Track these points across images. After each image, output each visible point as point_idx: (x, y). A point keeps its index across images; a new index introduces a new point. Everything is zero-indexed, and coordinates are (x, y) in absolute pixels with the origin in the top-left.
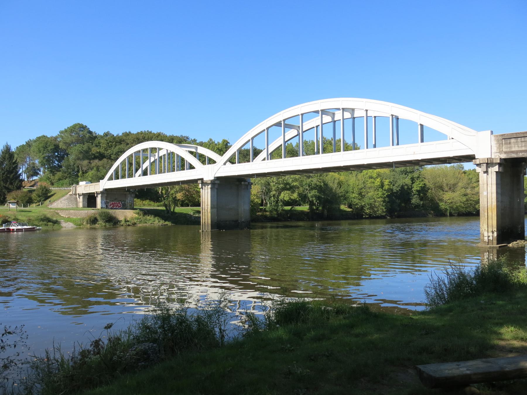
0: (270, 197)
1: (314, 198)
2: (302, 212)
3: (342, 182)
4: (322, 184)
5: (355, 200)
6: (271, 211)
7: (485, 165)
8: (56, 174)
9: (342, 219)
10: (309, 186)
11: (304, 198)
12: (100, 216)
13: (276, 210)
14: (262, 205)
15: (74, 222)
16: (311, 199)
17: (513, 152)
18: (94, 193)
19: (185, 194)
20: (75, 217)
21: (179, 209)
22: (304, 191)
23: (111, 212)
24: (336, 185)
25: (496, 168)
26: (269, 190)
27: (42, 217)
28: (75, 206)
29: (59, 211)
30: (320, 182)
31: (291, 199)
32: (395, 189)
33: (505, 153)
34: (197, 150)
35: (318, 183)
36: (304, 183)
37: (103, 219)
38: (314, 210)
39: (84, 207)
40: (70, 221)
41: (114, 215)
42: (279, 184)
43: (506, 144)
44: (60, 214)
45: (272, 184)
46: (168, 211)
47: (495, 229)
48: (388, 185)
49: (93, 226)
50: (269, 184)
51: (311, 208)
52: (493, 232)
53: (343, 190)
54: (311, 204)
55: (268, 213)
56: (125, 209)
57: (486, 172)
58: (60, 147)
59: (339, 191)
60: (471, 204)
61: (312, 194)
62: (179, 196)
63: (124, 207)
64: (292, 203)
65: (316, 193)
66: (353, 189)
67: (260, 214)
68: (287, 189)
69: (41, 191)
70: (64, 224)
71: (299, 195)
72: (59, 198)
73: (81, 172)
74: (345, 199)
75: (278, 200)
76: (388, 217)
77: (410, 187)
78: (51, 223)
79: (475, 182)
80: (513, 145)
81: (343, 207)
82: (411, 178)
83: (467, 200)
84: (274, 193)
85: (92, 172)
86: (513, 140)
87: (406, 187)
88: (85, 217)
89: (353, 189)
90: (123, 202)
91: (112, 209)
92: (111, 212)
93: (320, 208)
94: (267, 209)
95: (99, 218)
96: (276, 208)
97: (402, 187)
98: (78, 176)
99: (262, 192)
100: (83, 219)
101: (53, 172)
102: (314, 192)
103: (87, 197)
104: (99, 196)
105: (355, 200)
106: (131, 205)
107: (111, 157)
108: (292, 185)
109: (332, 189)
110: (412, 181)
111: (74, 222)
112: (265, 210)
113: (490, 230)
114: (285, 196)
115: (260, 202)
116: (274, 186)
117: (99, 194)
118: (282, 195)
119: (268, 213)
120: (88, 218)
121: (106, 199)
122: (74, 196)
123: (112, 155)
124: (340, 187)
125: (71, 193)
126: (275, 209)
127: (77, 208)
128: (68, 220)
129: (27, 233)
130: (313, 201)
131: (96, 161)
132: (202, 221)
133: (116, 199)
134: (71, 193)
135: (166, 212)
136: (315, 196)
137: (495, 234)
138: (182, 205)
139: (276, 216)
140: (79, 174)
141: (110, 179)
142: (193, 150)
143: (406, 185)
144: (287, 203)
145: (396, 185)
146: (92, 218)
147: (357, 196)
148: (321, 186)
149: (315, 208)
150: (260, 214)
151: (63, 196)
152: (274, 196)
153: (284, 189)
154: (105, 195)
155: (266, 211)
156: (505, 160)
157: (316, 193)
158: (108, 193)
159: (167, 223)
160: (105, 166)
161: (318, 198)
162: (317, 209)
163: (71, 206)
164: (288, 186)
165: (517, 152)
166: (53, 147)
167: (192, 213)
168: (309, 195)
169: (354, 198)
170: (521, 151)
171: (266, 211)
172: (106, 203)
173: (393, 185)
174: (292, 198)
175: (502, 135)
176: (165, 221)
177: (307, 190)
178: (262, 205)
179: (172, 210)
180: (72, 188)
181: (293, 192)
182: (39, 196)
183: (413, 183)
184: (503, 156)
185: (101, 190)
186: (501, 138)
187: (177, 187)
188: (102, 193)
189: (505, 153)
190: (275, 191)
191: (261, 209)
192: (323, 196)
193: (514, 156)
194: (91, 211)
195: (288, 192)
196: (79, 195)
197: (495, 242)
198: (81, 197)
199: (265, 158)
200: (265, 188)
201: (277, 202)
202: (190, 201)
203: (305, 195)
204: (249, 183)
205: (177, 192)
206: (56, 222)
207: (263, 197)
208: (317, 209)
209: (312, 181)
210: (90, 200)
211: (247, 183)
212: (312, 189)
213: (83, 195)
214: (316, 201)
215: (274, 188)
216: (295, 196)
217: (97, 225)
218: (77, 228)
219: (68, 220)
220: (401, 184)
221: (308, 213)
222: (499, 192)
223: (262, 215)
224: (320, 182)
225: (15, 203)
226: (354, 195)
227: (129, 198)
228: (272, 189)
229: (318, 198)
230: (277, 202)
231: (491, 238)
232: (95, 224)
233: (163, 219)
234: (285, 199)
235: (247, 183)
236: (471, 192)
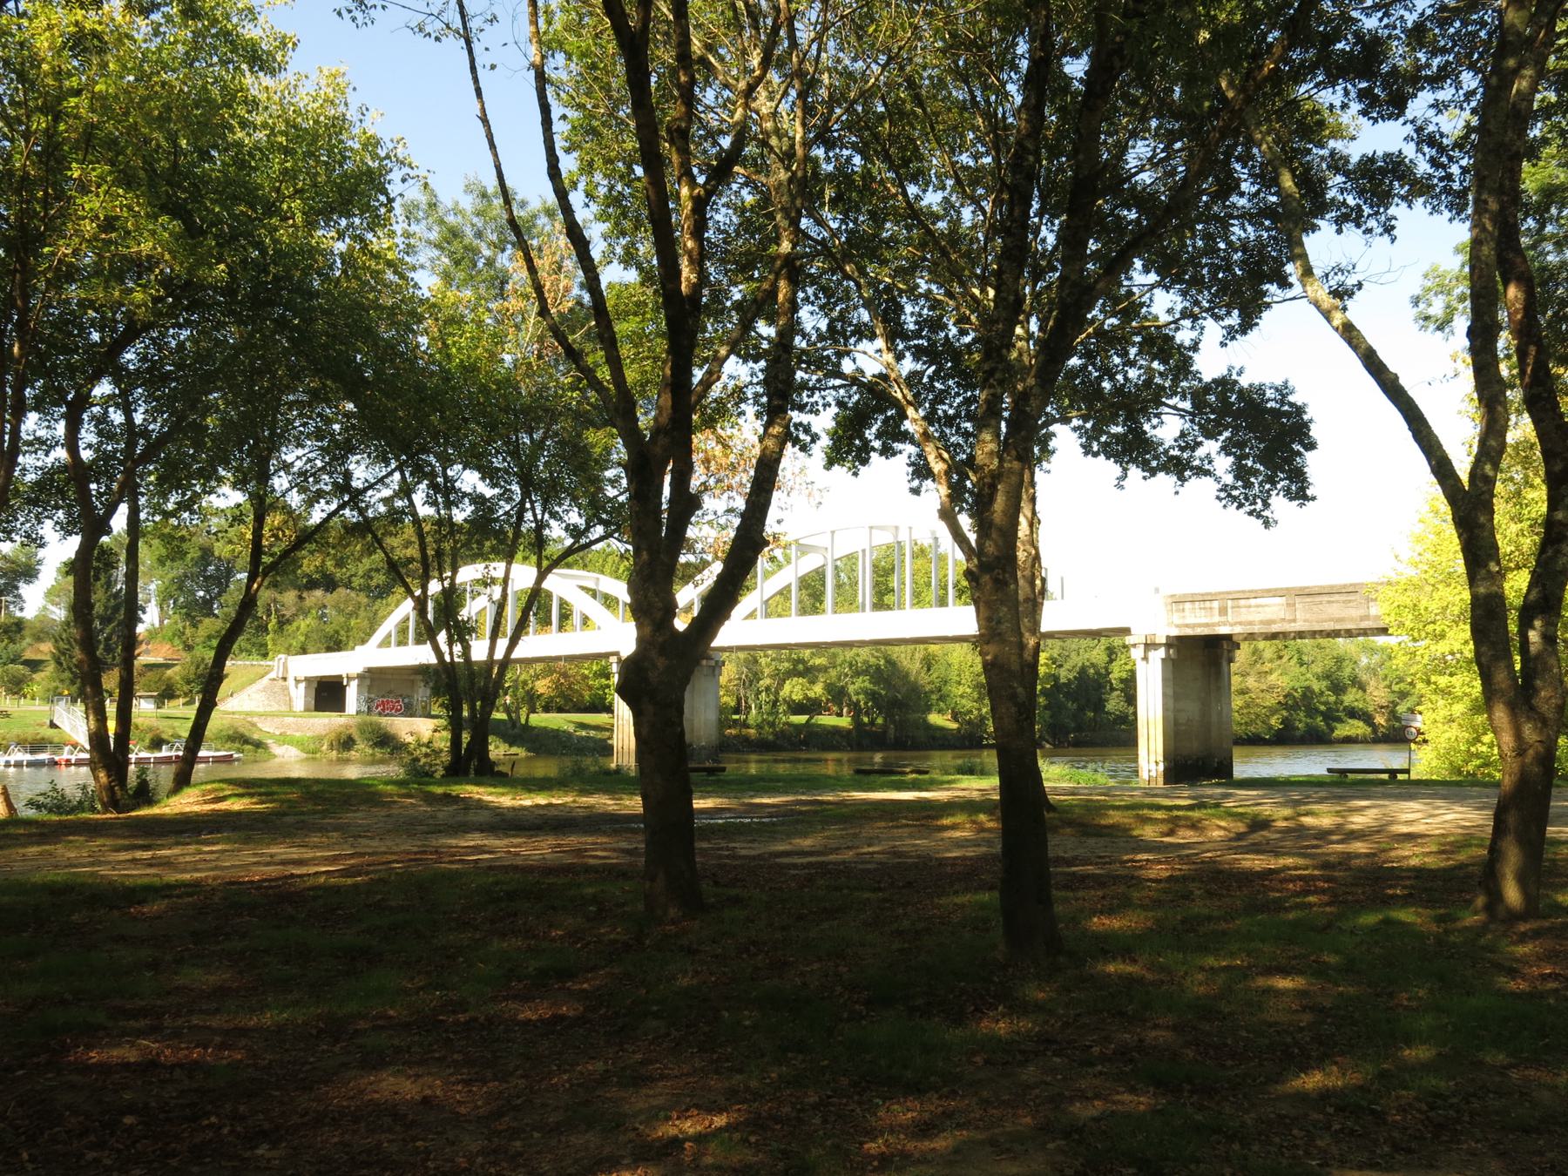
0: (759, 693)
1: (861, 697)
2: (836, 731)
3: (935, 656)
4: (882, 662)
5: (964, 701)
6: (759, 727)
7: (1142, 647)
8: (201, 621)
9: (933, 748)
10: (851, 665)
11: (837, 695)
12: (362, 732)
13: (772, 725)
14: (737, 710)
15: (299, 744)
16: (854, 698)
17: (1187, 626)
18: (340, 677)
19: (558, 685)
20: (298, 734)
21: (540, 719)
22: (839, 679)
23: (384, 720)
24: (918, 665)
25: (1161, 653)
26: (757, 677)
27: (231, 732)
28: (284, 708)
29: (255, 719)
30: (877, 658)
31: (809, 699)
32: (1065, 675)
33: (1177, 626)
34: (597, 584)
35: (872, 661)
36: (839, 661)
37: (368, 740)
38: (865, 724)
39: (307, 709)
40: (291, 743)
41: (393, 731)
42: (781, 661)
43: (1178, 611)
44: (259, 725)
45: (763, 661)
46: (513, 723)
47: (1161, 758)
48: (1046, 664)
49: (345, 755)
50: (756, 661)
51: (856, 720)
52: (1157, 763)
53: (935, 676)
54: (856, 709)
55: (752, 731)
56: (411, 716)
57: (1145, 658)
58: (216, 554)
59: (924, 679)
60: (1258, 716)
61: (857, 687)
62: (543, 686)
63: (409, 711)
64: (809, 707)
65: (867, 684)
66: (959, 675)
67: (733, 732)
68: (800, 674)
69: (193, 668)
70: (276, 750)
71: (829, 688)
72: (243, 687)
73: (274, 621)
74: (942, 698)
75: (776, 701)
76: (1048, 746)
77: (1103, 671)
78: (249, 747)
79: (1271, 661)
80: (1187, 613)
81: (935, 719)
82: (1108, 648)
83: (1248, 706)
84: (766, 682)
85: (308, 621)
86: (1188, 606)
87: (1092, 671)
88: (324, 733)
89: (959, 675)
90: (406, 700)
91: (380, 714)
92: (384, 720)
93: (880, 721)
94: (751, 721)
95: (356, 736)
96: (771, 719)
97: (1083, 670)
98: (266, 630)
99: (740, 679)
100: (320, 739)
101: (194, 618)
102: (862, 683)
103: (315, 685)
104: (354, 685)
105: (964, 701)
106: (424, 708)
107: (350, 582)
108: (811, 663)
109: (907, 675)
110: (1109, 656)
111: (299, 744)
112: (745, 725)
113: (1152, 759)
114: (794, 689)
115: (733, 704)
116: (768, 665)
117: (354, 679)
118: (787, 687)
119: (752, 731)
120: (333, 736)
121: (369, 692)
122: (281, 682)
123: (354, 579)
124: (929, 670)
125: (273, 675)
126: (768, 723)
127: (290, 712)
128: (283, 739)
129: (216, 765)
130: (858, 701)
131: (319, 593)
132: (615, 742)
133: (390, 692)
134: (273, 675)
135: (509, 726)
136: (865, 692)
137: (1161, 767)
138: (547, 709)
139: (771, 737)
140: (270, 627)
141: (385, 643)
142: (591, 585)
143: (1093, 665)
144: (797, 708)
145: (1067, 666)
146: (343, 737)
147: (969, 690)
148: (878, 667)
149: (866, 720)
150: (733, 732)
151: (252, 682)
152: (768, 689)
153: (792, 673)
154: (368, 682)
155: (748, 727)
156: (1179, 638)
157: (867, 684)
158: (375, 679)
159: (514, 750)
160: (342, 606)
161: (872, 696)
162: (872, 722)
163: (275, 708)
164: (801, 667)
165: (1194, 626)
166: (199, 553)
167: (571, 728)
168: (851, 689)
169: (962, 696)
170: (1200, 625)
171: (748, 727)
172: (369, 701)
173: (1061, 666)
174: (811, 694)
175: (1172, 596)
176: (511, 746)
177: (846, 675)
178: (737, 710)
179: (523, 721)
180: (276, 663)
181: (812, 682)
182: (188, 682)
183: (1111, 661)
184: (1175, 632)
185: (360, 670)
186: (1170, 600)
187: (539, 667)
188: (360, 677)
189: (1177, 626)
190: (771, 676)
191: (735, 721)
192: (883, 692)
193: (1189, 632)
194: (327, 722)
195: (801, 680)
196: (297, 681)
197: (1161, 780)
198: (302, 686)
199: (755, 610)
200: (745, 670)
201: (775, 703)
202: (567, 699)
203: (843, 687)
204: (717, 662)
205: (537, 677)
206: (258, 745)
207: (742, 692)
208: (872, 722)
209: (858, 655)
210: (328, 693)
211: (713, 663)
212: (858, 674)
213: (308, 680)
214: (866, 703)
215: (767, 671)
216: (818, 690)
217: (353, 753)
218: (307, 759)
219: (283, 739)
220: (1080, 664)
221: (849, 732)
222: (1170, 692)
223: (735, 737)
224: (877, 658)
225: (151, 697)
226: (961, 690)
227: (421, 690)
228: (762, 673)
229: (872, 696)
230: (775, 703)
231: (1153, 774)
232: (349, 750)
233: (505, 742)
234: (794, 697)
235: (713, 663)
236: (1256, 684)
